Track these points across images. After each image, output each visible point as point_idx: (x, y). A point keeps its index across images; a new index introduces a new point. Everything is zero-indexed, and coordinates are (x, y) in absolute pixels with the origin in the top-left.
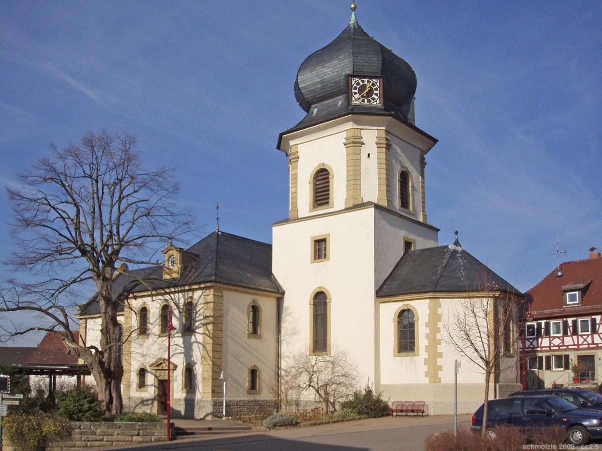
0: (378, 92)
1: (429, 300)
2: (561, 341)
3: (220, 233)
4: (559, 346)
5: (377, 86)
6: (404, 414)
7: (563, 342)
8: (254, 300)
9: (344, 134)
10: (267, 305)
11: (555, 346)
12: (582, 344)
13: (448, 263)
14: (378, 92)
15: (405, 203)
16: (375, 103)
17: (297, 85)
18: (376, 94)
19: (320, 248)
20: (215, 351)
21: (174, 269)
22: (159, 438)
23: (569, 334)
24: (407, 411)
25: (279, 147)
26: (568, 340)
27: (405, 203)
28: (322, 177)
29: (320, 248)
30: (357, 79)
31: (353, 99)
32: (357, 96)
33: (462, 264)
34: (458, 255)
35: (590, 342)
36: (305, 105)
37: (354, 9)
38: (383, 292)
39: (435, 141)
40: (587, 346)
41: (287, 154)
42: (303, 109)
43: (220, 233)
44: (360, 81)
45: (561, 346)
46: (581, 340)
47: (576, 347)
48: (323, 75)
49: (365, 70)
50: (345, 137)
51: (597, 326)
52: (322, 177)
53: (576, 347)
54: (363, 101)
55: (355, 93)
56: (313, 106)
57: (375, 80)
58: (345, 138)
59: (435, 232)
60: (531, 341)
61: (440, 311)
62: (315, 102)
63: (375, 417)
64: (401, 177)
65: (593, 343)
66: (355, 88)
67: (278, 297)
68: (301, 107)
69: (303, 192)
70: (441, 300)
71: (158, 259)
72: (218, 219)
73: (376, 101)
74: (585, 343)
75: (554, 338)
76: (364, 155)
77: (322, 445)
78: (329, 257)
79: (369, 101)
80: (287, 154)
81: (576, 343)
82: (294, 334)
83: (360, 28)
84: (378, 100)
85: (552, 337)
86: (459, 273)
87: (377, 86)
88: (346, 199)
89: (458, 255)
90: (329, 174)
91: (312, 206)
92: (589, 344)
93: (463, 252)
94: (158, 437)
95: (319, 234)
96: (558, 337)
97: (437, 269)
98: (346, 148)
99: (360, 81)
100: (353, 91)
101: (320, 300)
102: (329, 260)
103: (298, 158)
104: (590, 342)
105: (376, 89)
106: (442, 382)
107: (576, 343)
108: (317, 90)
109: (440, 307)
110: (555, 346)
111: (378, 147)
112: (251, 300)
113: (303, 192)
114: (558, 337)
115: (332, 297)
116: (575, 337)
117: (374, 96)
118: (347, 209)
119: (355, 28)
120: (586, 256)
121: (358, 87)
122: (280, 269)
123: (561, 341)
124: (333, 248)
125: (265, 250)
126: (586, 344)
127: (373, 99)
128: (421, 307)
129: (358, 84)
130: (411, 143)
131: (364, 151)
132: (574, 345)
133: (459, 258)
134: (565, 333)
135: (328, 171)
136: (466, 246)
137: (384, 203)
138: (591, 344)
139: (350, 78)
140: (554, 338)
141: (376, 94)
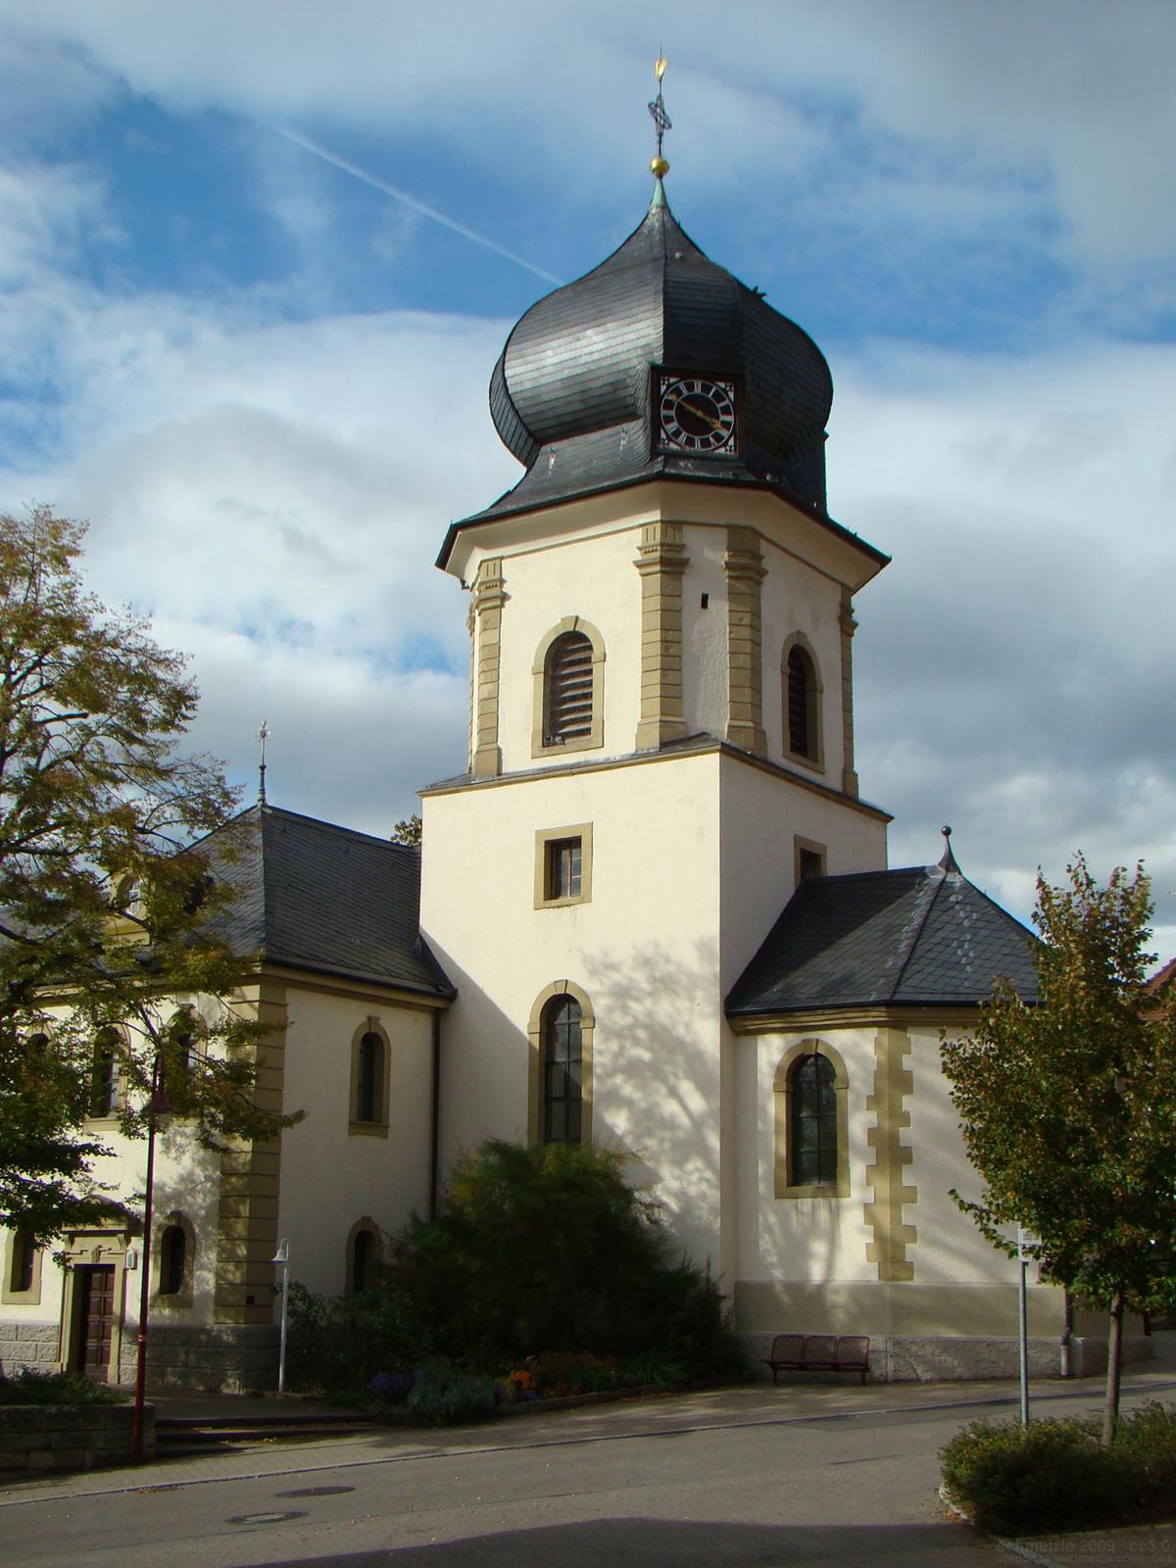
0: (730, 418)
1: (876, 1030)
3: (270, 811)
5: (727, 402)
8: (369, 1018)
9: (637, 537)
10: (406, 1034)
13: (926, 919)
14: (730, 418)
16: (722, 450)
18: (726, 425)
19: (561, 864)
20: (270, 1197)
21: (128, 930)
25: (442, 563)
29: (561, 864)
31: (663, 436)
32: (672, 427)
34: (953, 899)
36: (521, 444)
41: (463, 582)
42: (513, 453)
43: (270, 811)
44: (682, 386)
50: (640, 545)
54: (690, 442)
56: (546, 448)
57: (722, 385)
58: (640, 549)
59: (878, 823)
62: (553, 436)
64: (790, 664)
67: (437, 1009)
68: (508, 447)
73: (669, 386)
79: (705, 443)
80: (463, 582)
82: (146, 627)
83: (677, 226)
84: (731, 442)
86: (960, 952)
87: (727, 402)
88: (639, 725)
89: (953, 899)
90: (590, 648)
97: (896, 936)
98: (643, 575)
99: (682, 386)
100: (663, 412)
102: (538, 833)
112: (363, 1019)
119: (664, 232)
120: (752, 288)
122: (442, 918)
124: (601, 866)
125: (399, 865)
127: (677, 434)
130: (818, 566)
133: (957, 907)
135: (588, 640)
137: (743, 742)
141: (726, 425)
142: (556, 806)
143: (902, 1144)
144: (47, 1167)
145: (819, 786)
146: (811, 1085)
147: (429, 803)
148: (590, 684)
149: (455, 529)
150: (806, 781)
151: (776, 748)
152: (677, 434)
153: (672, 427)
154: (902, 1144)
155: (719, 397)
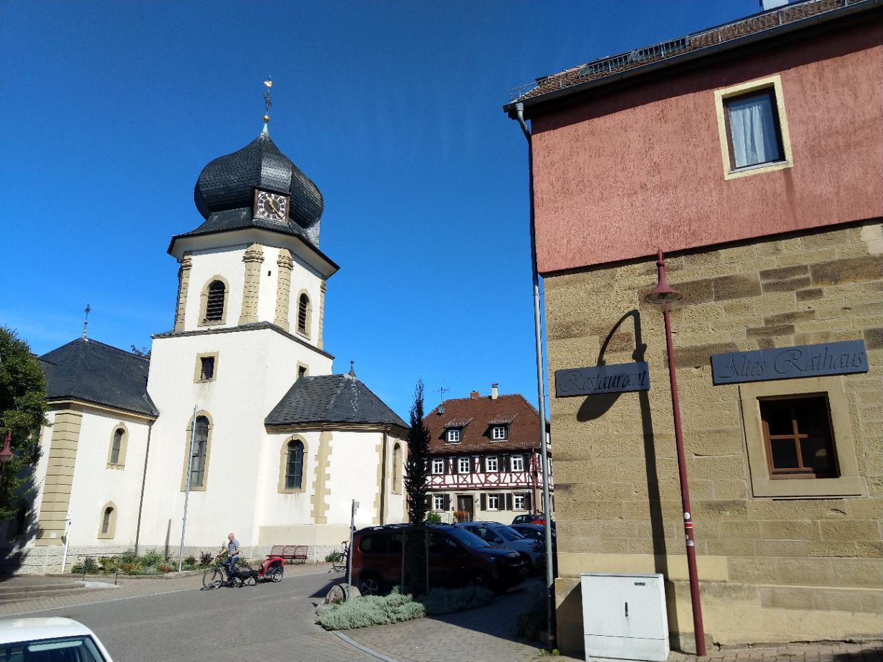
0: (284, 209)
2: (488, 479)
4: (440, 485)
5: (283, 204)
7: (444, 481)
11: (436, 485)
12: (462, 484)
14: (284, 209)
15: (302, 324)
19: (208, 365)
23: (450, 472)
25: (170, 251)
26: (449, 479)
27: (302, 324)
28: (217, 290)
29: (208, 365)
30: (264, 193)
33: (356, 394)
35: (470, 482)
37: (267, 121)
39: (337, 268)
40: (466, 486)
45: (442, 485)
46: (461, 480)
47: (456, 486)
51: (476, 465)
52: (217, 290)
53: (456, 486)
54: (268, 216)
60: (518, 475)
61: (331, 444)
65: (472, 483)
66: (262, 202)
70: (333, 432)
71: (354, 361)
72: (86, 323)
74: (465, 482)
75: (490, 473)
76: (264, 273)
78: (215, 377)
79: (274, 217)
81: (456, 482)
85: (488, 473)
87: (283, 204)
91: (202, 320)
92: (467, 484)
93: (358, 382)
95: (207, 351)
96: (495, 473)
101: (202, 424)
104: (470, 482)
105: (283, 207)
106: (328, 523)
107: (456, 482)
108: (232, 198)
109: (332, 439)
110: (436, 485)
114: (495, 473)
115: (214, 423)
116: (455, 476)
117: (266, 214)
118: (242, 328)
121: (264, 201)
123: (488, 479)
125: (140, 362)
126: (465, 484)
127: (264, 213)
128: (311, 439)
131: (264, 268)
132: (454, 484)
134: (446, 473)
136: (362, 377)
138: (470, 484)
139: (257, 191)
140: (490, 473)
141: (283, 212)
142: (207, 344)
143: (407, 521)
144: (270, 206)
145: (308, 344)
146: (296, 449)
147: (156, 342)
148: (209, 306)
149: (174, 239)
150: (302, 341)
151: (293, 329)
152: (264, 213)
153: (261, 210)
154: (407, 521)
155: (281, 202)
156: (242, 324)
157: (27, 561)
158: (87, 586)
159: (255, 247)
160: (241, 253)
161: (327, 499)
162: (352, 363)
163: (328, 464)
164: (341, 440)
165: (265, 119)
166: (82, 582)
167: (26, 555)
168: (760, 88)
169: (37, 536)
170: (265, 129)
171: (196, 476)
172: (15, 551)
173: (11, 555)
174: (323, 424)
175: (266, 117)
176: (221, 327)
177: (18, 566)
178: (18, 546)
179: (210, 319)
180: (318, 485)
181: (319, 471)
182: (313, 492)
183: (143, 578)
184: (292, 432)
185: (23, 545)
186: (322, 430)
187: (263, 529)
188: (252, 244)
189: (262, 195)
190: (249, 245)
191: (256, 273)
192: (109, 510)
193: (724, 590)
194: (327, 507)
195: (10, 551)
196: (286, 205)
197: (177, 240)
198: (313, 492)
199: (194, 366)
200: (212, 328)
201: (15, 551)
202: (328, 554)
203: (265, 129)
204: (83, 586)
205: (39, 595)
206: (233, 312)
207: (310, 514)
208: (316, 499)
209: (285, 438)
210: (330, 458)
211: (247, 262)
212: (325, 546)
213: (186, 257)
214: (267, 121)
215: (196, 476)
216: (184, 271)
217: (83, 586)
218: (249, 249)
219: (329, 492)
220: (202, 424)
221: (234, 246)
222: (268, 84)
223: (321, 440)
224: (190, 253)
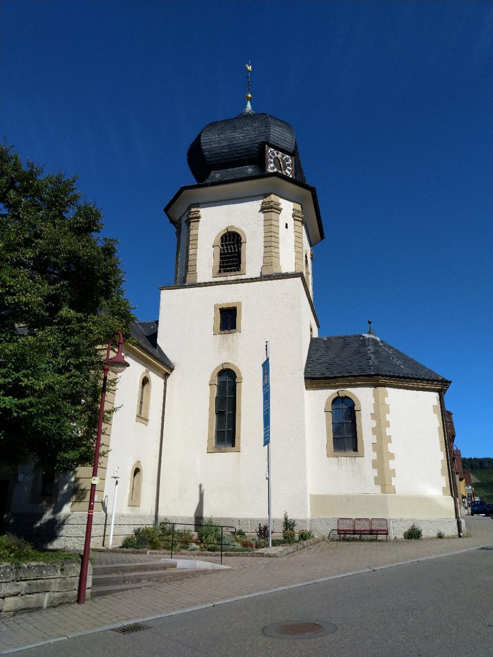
6: (357, 536)
17: (199, 136)
19: (228, 318)
22: (63, 597)
24: (361, 533)
29: (228, 318)
30: (272, 150)
38: (313, 380)
44: (275, 152)
48: (232, 140)
49: (280, 143)
55: (271, 163)
61: (387, 401)
63: (424, 367)
69: (205, 257)
70: (388, 389)
77: (168, 204)
94: (61, 594)
101: (227, 383)
102: (240, 303)
103: (199, 217)
108: (223, 154)
111: (295, 220)
113: (205, 257)
124: (243, 320)
128: (363, 396)
129: (273, 154)
141: (289, 170)
142: (227, 295)
152: (273, 168)
156: (265, 273)
157: (65, 531)
158: (179, 566)
159: (273, 197)
160: (257, 204)
161: (392, 464)
162: (370, 323)
163: (388, 424)
164: (395, 397)
165: (248, 97)
166: (173, 561)
167: (63, 523)
168: (142, 362)
169: (78, 498)
170: (249, 105)
171: (226, 433)
172: (48, 516)
173: (42, 521)
174: (376, 378)
175: (250, 96)
176: (240, 277)
177: (54, 536)
178: (51, 510)
179: (225, 271)
180: (380, 447)
181: (379, 431)
182: (374, 456)
183: (235, 555)
184: (336, 387)
185: (58, 509)
186: (375, 386)
187: (311, 496)
188: (269, 194)
189: (271, 151)
190: (266, 195)
191: (274, 223)
192: (137, 471)
193: (174, 554)
194: (393, 473)
195: (40, 516)
196: (292, 164)
197: (185, 192)
198: (374, 456)
199: (211, 319)
200: (230, 278)
201: (48, 516)
202: (407, 530)
203: (249, 105)
204: (174, 566)
205: (139, 580)
206: (252, 261)
207: (373, 481)
208: (380, 464)
209: (326, 395)
210: (388, 417)
211: (265, 212)
212: (401, 520)
213: (193, 210)
214: (250, 99)
215: (226, 433)
216: (192, 223)
217: (174, 566)
218: (268, 199)
219: (392, 456)
220: (227, 383)
221: (248, 197)
222: (250, 68)
223: (376, 396)
224: (197, 205)
